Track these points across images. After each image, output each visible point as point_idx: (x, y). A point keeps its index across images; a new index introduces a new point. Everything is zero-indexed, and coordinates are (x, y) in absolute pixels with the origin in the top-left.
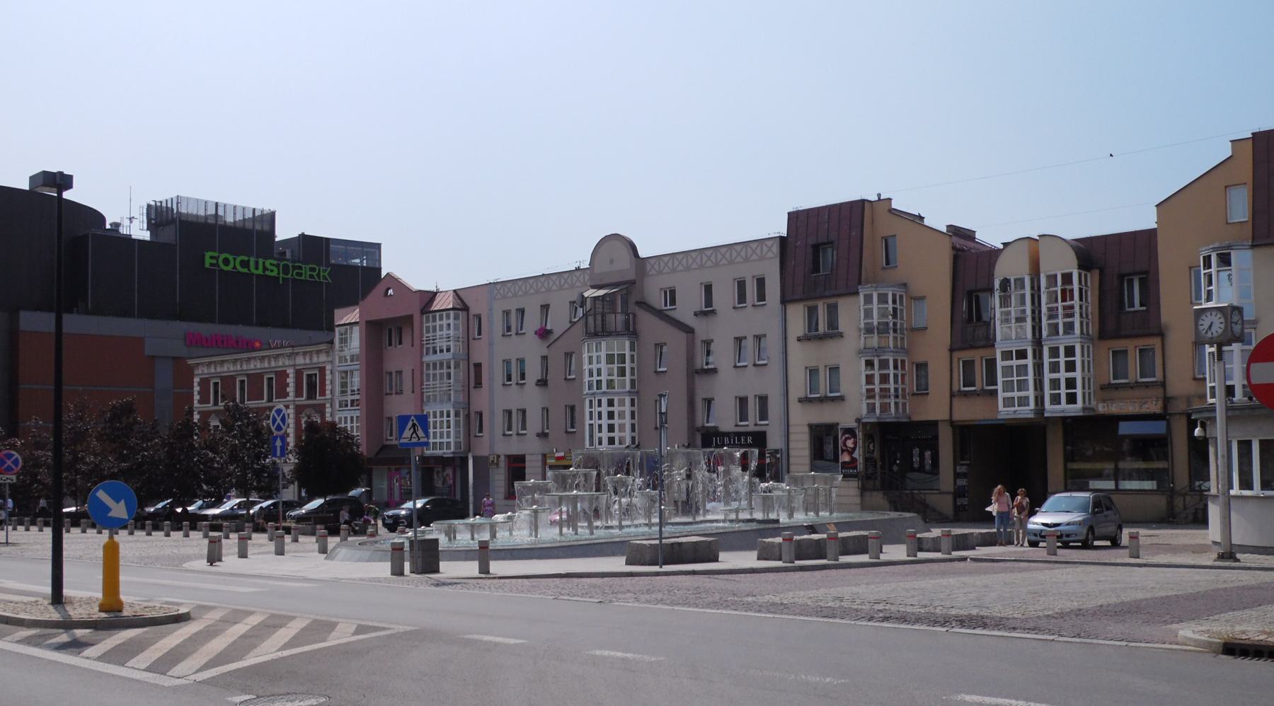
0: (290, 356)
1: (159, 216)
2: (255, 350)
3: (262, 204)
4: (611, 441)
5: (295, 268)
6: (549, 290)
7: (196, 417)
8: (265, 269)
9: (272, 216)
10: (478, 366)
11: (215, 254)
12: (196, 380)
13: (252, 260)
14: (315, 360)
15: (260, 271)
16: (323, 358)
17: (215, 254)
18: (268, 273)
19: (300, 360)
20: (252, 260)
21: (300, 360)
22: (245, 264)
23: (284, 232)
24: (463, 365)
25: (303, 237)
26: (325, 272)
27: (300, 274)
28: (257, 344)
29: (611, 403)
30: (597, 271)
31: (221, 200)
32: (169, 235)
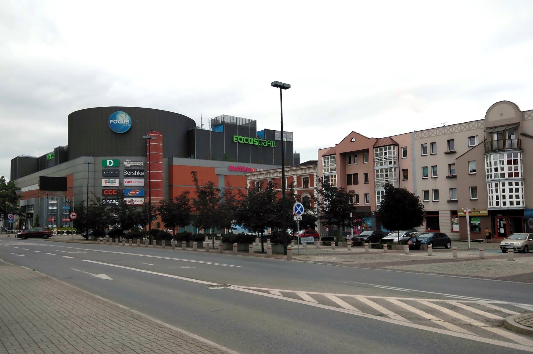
0: (294, 171)
1: (215, 123)
2: (253, 172)
3: (253, 119)
4: (511, 203)
5: (264, 142)
6: (453, 132)
7: (296, 193)
8: (254, 142)
9: (256, 121)
10: (405, 171)
11: (237, 136)
12: (248, 182)
13: (249, 139)
14: (307, 171)
15: (252, 143)
16: (311, 171)
17: (237, 136)
18: (255, 144)
19: (299, 172)
20: (249, 139)
21: (299, 172)
22: (247, 140)
23: (260, 128)
24: (397, 170)
25: (265, 130)
26: (273, 143)
27: (265, 144)
28: (253, 170)
29: (510, 184)
30: (491, 119)
31: (238, 116)
32: (220, 129)
